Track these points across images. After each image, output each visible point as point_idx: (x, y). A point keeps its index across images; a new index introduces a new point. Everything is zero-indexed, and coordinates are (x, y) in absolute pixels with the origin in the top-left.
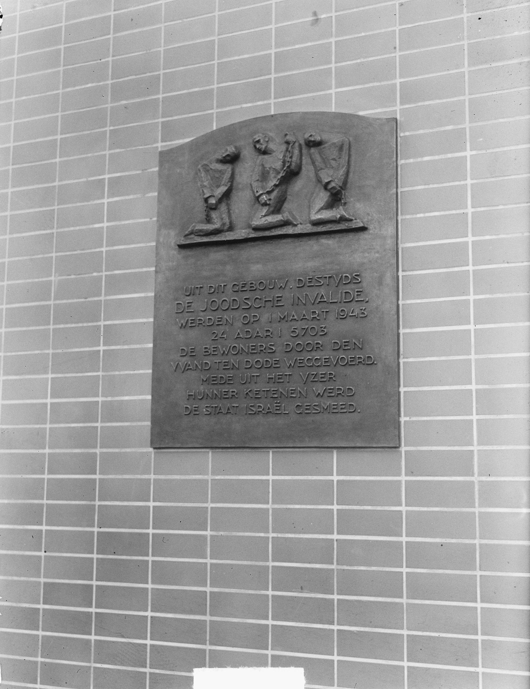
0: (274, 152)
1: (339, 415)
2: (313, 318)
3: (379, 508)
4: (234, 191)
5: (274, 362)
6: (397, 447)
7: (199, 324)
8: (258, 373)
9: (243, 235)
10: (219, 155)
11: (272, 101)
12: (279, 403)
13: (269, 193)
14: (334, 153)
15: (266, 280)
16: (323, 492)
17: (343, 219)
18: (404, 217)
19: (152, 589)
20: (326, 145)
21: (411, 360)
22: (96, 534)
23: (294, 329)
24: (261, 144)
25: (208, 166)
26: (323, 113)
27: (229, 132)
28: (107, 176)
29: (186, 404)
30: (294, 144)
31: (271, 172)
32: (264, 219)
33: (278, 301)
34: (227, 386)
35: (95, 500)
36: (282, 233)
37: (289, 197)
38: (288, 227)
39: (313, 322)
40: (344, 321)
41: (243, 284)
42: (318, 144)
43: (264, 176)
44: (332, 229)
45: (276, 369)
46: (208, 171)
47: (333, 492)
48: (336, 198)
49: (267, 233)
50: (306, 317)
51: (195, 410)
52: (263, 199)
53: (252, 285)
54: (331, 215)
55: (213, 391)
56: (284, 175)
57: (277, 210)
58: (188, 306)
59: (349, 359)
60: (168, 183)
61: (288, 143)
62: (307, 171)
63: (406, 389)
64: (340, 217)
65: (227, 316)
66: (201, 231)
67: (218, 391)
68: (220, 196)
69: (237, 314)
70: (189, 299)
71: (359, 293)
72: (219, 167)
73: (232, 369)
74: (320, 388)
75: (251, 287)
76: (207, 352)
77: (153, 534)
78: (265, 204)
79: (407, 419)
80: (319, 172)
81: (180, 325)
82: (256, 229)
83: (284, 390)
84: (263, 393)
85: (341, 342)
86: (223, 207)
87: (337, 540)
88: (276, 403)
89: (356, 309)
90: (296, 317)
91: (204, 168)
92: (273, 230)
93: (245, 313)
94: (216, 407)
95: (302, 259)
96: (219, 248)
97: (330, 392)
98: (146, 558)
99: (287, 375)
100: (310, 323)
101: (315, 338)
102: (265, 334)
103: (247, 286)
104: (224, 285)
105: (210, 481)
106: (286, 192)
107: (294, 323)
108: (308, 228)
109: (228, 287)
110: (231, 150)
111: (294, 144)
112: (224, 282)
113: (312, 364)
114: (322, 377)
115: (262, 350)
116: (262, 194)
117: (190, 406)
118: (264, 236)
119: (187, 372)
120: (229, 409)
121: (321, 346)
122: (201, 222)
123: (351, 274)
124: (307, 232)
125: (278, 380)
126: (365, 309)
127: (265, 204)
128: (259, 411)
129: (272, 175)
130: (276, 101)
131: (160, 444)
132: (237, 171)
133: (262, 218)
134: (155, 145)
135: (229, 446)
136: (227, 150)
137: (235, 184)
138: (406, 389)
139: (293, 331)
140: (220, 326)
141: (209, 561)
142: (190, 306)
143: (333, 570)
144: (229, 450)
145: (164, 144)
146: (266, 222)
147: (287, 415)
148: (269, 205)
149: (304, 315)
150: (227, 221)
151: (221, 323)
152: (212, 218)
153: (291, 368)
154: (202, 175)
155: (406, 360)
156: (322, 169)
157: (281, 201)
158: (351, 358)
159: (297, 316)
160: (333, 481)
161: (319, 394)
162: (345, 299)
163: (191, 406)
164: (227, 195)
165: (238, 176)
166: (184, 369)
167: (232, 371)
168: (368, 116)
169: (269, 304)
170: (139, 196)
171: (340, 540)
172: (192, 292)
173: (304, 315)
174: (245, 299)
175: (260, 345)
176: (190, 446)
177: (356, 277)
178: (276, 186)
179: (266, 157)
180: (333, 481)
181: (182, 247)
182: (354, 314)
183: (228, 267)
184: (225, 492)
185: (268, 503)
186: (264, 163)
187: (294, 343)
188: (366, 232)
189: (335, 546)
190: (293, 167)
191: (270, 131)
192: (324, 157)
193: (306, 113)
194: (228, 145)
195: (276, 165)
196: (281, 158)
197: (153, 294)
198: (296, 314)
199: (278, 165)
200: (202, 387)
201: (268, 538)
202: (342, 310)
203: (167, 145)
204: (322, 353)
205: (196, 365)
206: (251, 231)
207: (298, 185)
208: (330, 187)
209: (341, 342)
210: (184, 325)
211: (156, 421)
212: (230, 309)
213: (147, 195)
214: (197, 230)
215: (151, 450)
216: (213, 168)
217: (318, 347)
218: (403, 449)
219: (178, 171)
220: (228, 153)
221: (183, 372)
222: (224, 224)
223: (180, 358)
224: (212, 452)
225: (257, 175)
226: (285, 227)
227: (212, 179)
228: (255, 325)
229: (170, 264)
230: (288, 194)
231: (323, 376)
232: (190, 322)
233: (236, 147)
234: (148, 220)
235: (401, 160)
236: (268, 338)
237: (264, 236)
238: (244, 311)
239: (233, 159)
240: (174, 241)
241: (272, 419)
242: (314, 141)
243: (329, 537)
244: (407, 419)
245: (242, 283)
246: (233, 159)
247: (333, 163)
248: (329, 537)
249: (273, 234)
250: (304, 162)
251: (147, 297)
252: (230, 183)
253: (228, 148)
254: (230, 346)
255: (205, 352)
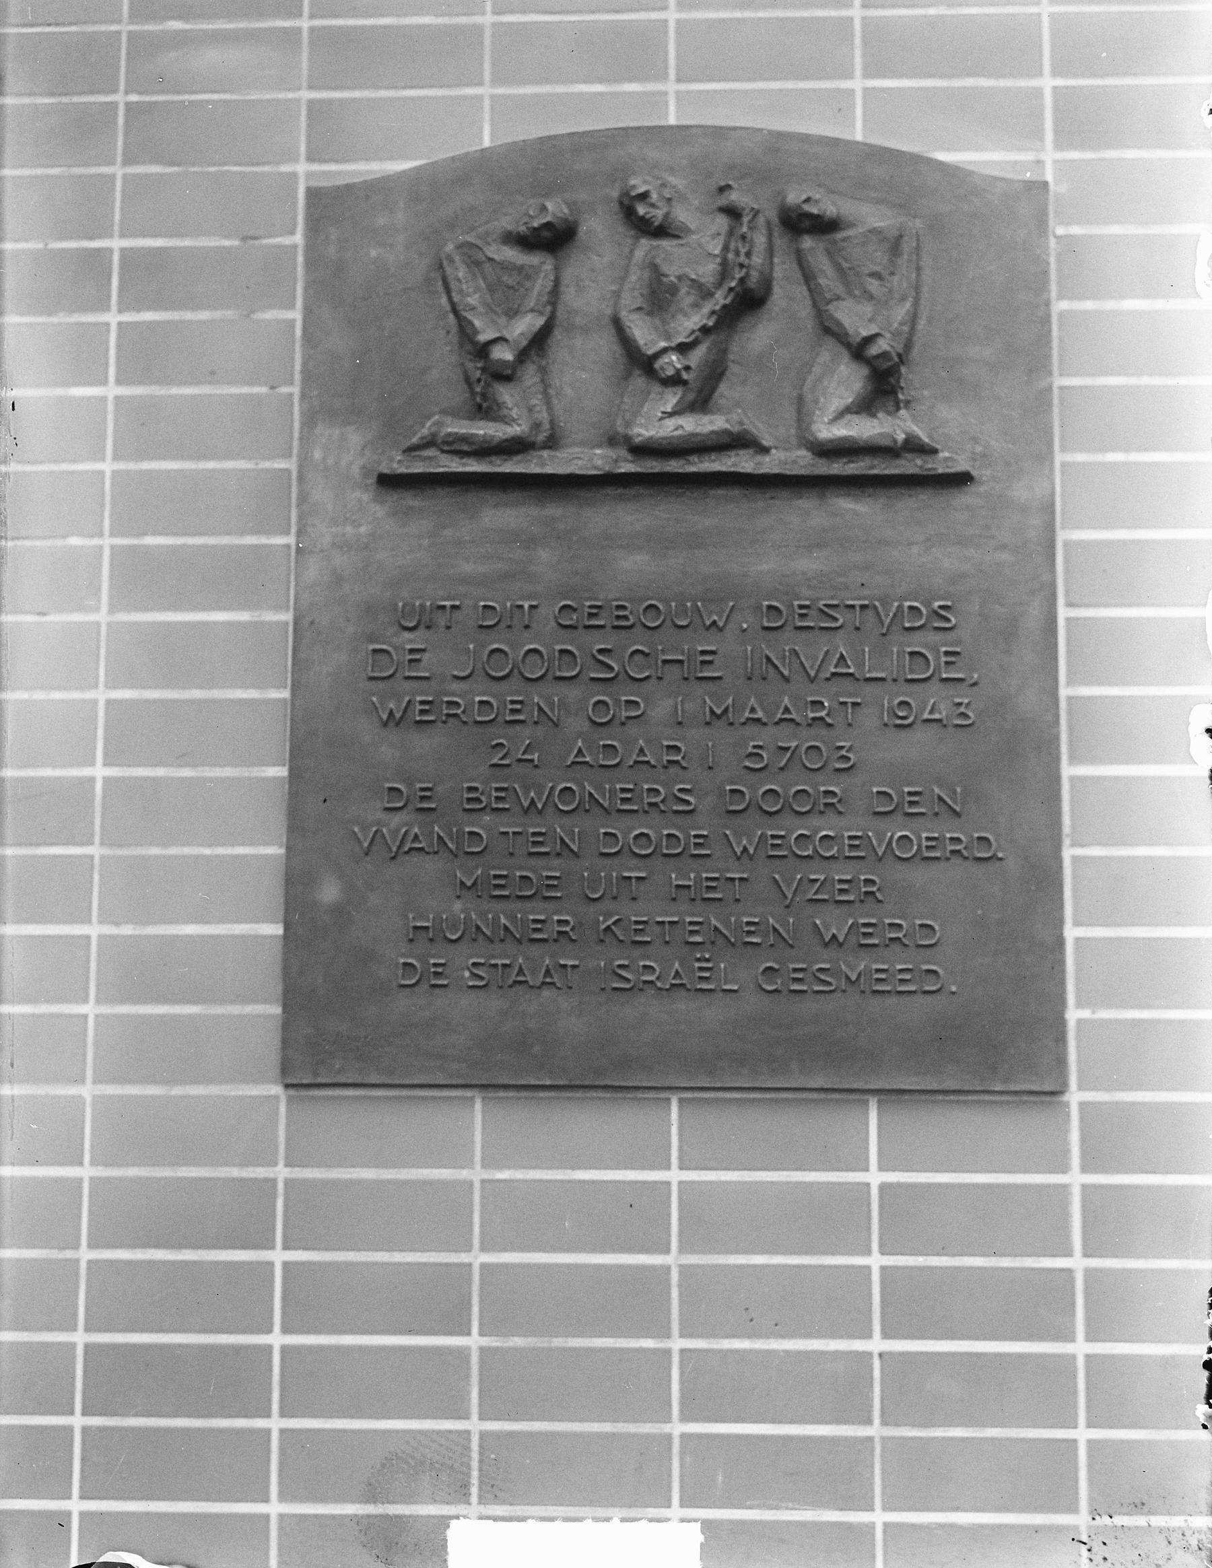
0: (688, 231)
1: (892, 1000)
2: (814, 719)
3: (1006, 1262)
4: (557, 333)
5: (693, 840)
6: (1052, 1095)
7: (448, 715)
8: (640, 870)
9: (599, 463)
10: (506, 223)
11: (671, 87)
12: (707, 960)
13: (683, 349)
14: (878, 258)
15: (666, 601)
16: (837, 1219)
17: (914, 447)
18: (1069, 457)
19: (282, 1517)
20: (850, 233)
21: (1095, 851)
22: (80, 1351)
23: (755, 747)
24: (653, 205)
25: (480, 249)
26: (835, 142)
27: (548, 161)
28: (116, 244)
29: (403, 955)
30: (755, 216)
31: (683, 291)
32: (670, 423)
33: (703, 662)
34: (541, 905)
35: (76, 1246)
36: (724, 469)
37: (733, 368)
38: (741, 452)
39: (813, 731)
40: (903, 734)
41: (591, 607)
42: (825, 226)
43: (660, 297)
44: (875, 472)
45: (701, 861)
46: (478, 264)
47: (869, 1218)
48: (884, 384)
49: (674, 466)
50: (793, 716)
51: (436, 973)
52: (671, 363)
53: (621, 613)
54: (878, 430)
55: (496, 919)
56: (728, 301)
57: (701, 403)
58: (411, 661)
59: (924, 843)
60: (328, 279)
61: (733, 213)
62: (788, 296)
63: (1081, 932)
64: (907, 441)
65: (541, 696)
66: (464, 439)
67: (512, 918)
68: (524, 343)
69: (572, 693)
70: (410, 640)
71: (952, 659)
72: (511, 254)
73: (558, 854)
74: (835, 924)
75: (618, 617)
76: (478, 800)
77: (285, 1350)
78: (675, 381)
79: (1085, 1014)
80: (831, 307)
81: (385, 717)
82: (642, 450)
83: (727, 924)
84: (657, 929)
85: (901, 794)
86: (530, 376)
87: (881, 1355)
88: (698, 960)
89: (936, 701)
90: (760, 714)
91: (464, 254)
92: (694, 458)
93: (598, 694)
94: (504, 966)
95: (785, 549)
96: (515, 496)
97: (865, 934)
98: (259, 1423)
99: (733, 879)
100: (803, 732)
101: (820, 777)
102: (666, 758)
103: (603, 613)
104: (532, 607)
105: (477, 1186)
106: (725, 351)
107: (752, 729)
108: (800, 461)
109: (543, 611)
110: (555, 209)
111: (755, 216)
112: (529, 598)
113: (810, 852)
114: (841, 891)
115: (655, 805)
116: (665, 351)
117: (419, 959)
118: (660, 474)
119: (407, 858)
120: (548, 973)
121: (839, 801)
122: (455, 413)
123: (928, 604)
124: (803, 472)
125: (702, 895)
126: (968, 704)
127: (675, 381)
128: (645, 982)
129: (686, 297)
130: (683, 87)
131: (316, 1074)
132: (568, 274)
133: (660, 419)
134: (285, 168)
135: (548, 1083)
136: (543, 208)
137: (561, 314)
138: (1081, 932)
139: (751, 755)
140: (518, 728)
141: (474, 1425)
142: (418, 660)
143: (870, 1439)
144: (541, 1094)
145: (316, 167)
146: (676, 433)
147: (734, 995)
148: (685, 383)
149: (787, 710)
150: (544, 416)
151: (521, 717)
152: (500, 406)
153: (745, 860)
154: (461, 275)
155: (1079, 851)
156: (838, 298)
157: (715, 373)
158: (928, 839)
159: (764, 710)
160: (868, 1185)
161: (834, 936)
162: (912, 671)
163: (423, 959)
164: (539, 341)
165: (572, 290)
166: (399, 847)
167: (556, 862)
168: (971, 168)
169: (673, 673)
170: (230, 314)
171: (891, 1354)
172: (425, 618)
173: (787, 710)
174: (600, 651)
175: (649, 790)
176: (416, 1082)
177: (943, 613)
178: (705, 330)
179: (665, 243)
180: (868, 1185)
181: (388, 482)
182: (937, 716)
183: (544, 554)
184: (521, 1218)
185: (667, 1251)
186: (658, 261)
187: (754, 788)
188: (972, 488)
189: (877, 1373)
190: (753, 282)
191: (671, 170)
192: (845, 265)
193: (780, 135)
194: (547, 195)
195: (701, 270)
196: (717, 252)
197: (287, 617)
198: (761, 705)
199: (707, 271)
200: (457, 906)
201: (668, 1352)
202: (902, 703)
203: (323, 173)
204: (842, 822)
205: (439, 837)
206: (623, 453)
207: (759, 335)
208: (873, 350)
209: (901, 794)
210: (398, 715)
211: (297, 998)
212: (549, 677)
213: (259, 316)
214: (450, 434)
215: (277, 1090)
216: (496, 257)
217: (831, 805)
218: (1075, 1097)
219: (373, 253)
220: (548, 219)
221: (393, 858)
222: (537, 426)
223: (384, 816)
224: (484, 1099)
225: (636, 293)
226: (733, 453)
227: (491, 289)
228: (632, 730)
229: (349, 529)
230: (731, 357)
231: (845, 886)
232: (419, 707)
233: (571, 205)
234: (263, 390)
235: (1058, 299)
236: (673, 770)
237: (660, 474)
238: (597, 687)
239: (554, 239)
240: (360, 462)
241: (683, 1005)
242: (818, 216)
243: (858, 1345)
244: (1085, 1014)
245: (588, 604)
246: (554, 239)
247: (873, 285)
248: (858, 1345)
249: (693, 469)
250: (778, 273)
251: (262, 623)
252: (549, 308)
253: (550, 206)
254: (552, 788)
255: (469, 800)
